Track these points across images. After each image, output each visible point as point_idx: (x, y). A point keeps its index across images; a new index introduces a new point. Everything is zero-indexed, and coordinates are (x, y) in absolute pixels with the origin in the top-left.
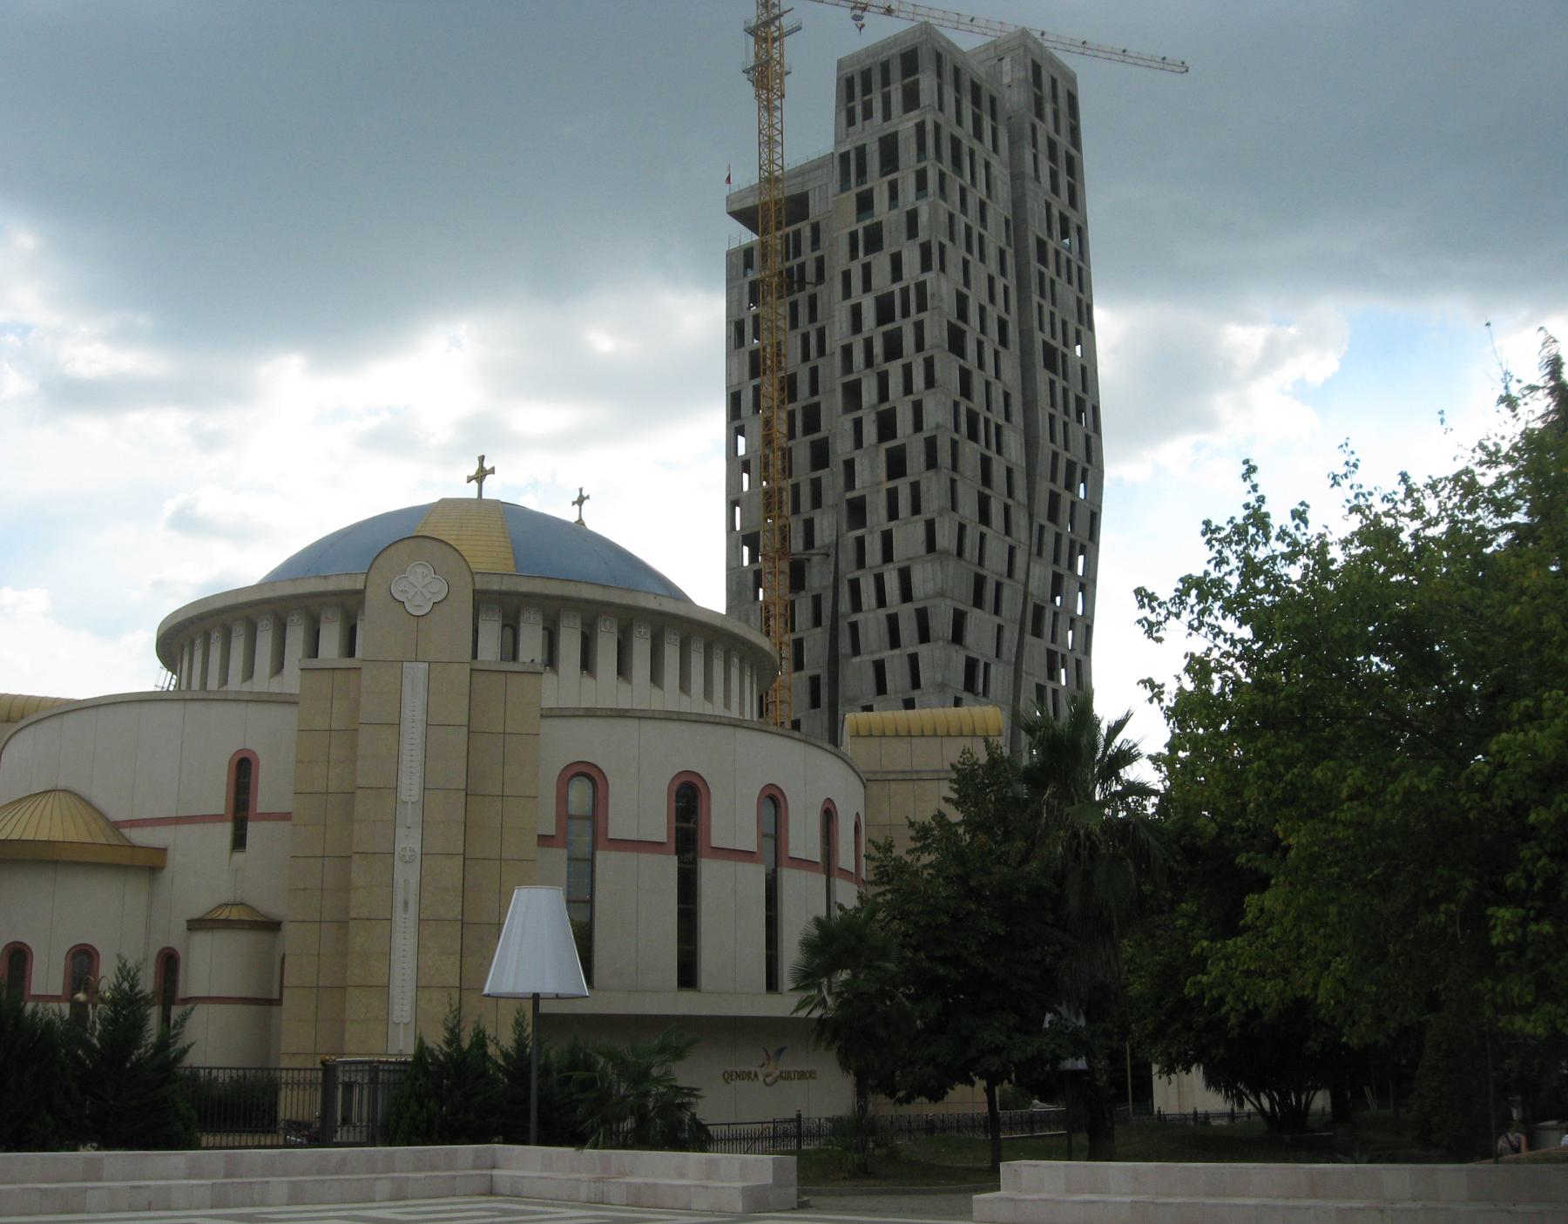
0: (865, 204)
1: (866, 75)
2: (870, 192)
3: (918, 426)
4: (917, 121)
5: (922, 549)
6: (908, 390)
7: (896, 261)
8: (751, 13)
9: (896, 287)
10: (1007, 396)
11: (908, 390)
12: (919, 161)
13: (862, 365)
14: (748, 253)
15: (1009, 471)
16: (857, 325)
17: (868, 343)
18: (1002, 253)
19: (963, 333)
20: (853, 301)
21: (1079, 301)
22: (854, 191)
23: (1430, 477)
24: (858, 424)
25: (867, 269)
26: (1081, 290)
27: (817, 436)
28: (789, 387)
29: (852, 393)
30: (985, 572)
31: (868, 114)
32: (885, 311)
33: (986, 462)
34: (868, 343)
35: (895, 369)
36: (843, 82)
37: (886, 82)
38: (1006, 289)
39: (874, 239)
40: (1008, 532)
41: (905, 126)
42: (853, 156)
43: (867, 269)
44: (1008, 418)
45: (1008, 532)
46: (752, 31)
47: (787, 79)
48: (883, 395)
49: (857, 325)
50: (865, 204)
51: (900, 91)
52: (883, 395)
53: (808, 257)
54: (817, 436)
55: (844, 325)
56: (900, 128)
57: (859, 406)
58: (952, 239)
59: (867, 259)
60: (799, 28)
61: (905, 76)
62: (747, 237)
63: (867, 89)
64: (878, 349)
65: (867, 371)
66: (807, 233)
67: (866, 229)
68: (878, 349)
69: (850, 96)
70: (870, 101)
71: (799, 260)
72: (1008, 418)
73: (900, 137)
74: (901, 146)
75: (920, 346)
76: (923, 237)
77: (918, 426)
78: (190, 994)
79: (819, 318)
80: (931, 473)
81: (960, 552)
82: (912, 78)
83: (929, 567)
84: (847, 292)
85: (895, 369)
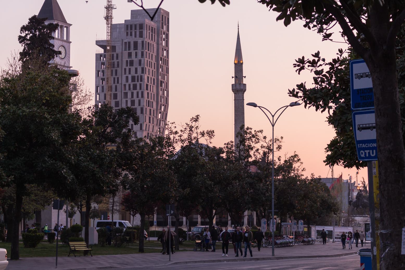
0: (130, 55)
1: (131, 26)
2: (131, 53)
3: (139, 105)
4: (142, 40)
5: (139, 129)
6: (138, 97)
7: (136, 69)
8: (105, 4)
9: (136, 75)
10: (154, 95)
11: (138, 97)
12: (142, 49)
13: (128, 90)
14: (101, 55)
15: (154, 110)
16: (127, 81)
17: (130, 85)
18: (155, 63)
19: (148, 85)
20: (126, 75)
21: (167, 68)
22: (127, 51)
23: (233, 77)
24: (127, 101)
25: (130, 69)
26: (167, 66)
27: (116, 100)
28: (110, 88)
29: (126, 94)
30: (149, 132)
31: (131, 35)
32: (133, 79)
33: (150, 110)
34: (130, 85)
35: (135, 92)
36: (126, 26)
37: (136, 29)
38: (155, 71)
39: (132, 63)
40: (153, 123)
41: (140, 40)
42: (127, 43)
43: (130, 69)
44: (154, 100)
45: (153, 123)
46: (106, 8)
47: (113, 19)
48: (132, 96)
49: (127, 81)
50: (130, 55)
51: (139, 32)
52: (132, 96)
53: (115, 61)
54: (116, 100)
55: (124, 80)
56: (138, 41)
57: (127, 98)
58: (147, 66)
59: (130, 67)
60: (116, 8)
61: (140, 29)
62: (101, 51)
63: (131, 29)
64: (132, 87)
65: (129, 91)
66: (115, 55)
67: (130, 61)
68: (132, 87)
69: (127, 29)
70: (132, 32)
71: (113, 61)
72: (154, 100)
73: (138, 43)
74: (138, 45)
75: (140, 89)
76: (142, 66)
77: (139, 105)
78: (275, 250)
79: (118, 75)
80: (141, 115)
81: (146, 130)
82: (141, 30)
83: (140, 133)
84: (125, 73)
85: (135, 92)
